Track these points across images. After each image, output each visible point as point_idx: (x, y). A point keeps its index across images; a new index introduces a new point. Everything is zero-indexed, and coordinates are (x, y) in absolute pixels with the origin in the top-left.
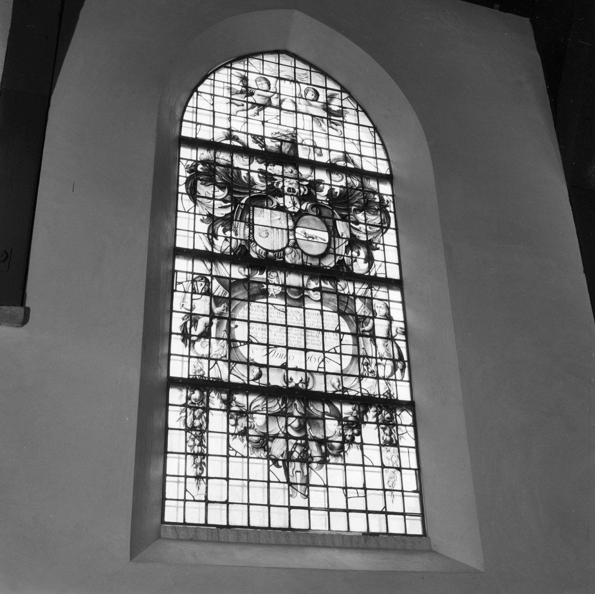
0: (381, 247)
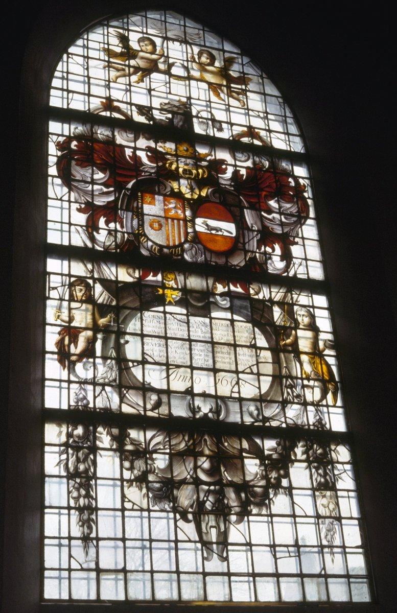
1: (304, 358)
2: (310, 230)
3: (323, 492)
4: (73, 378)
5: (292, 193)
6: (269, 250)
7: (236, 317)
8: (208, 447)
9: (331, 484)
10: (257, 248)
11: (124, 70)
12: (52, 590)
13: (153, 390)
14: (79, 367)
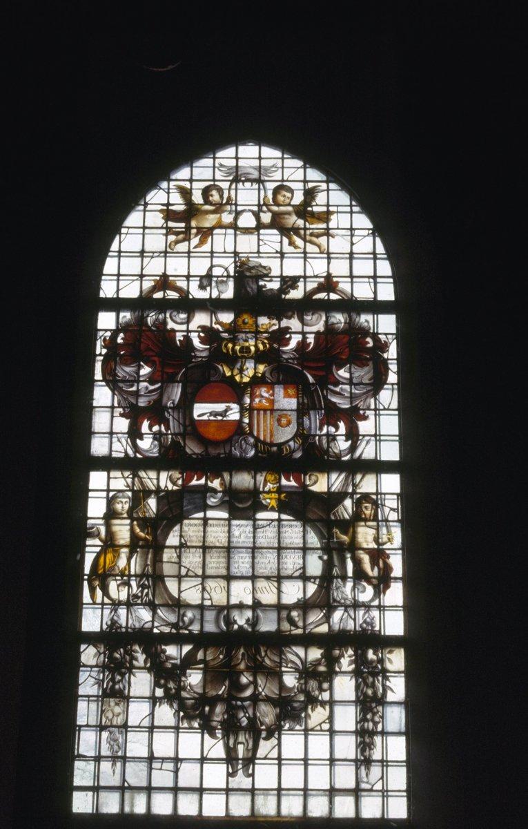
0: (370, 413)
2: (388, 397)
6: (332, 429)
7: (284, 517)
12: (81, 804)
13: (189, 606)
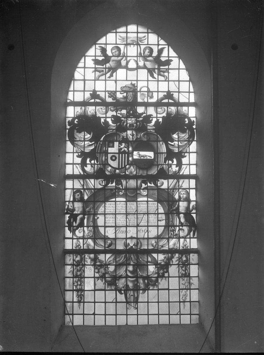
1: (182, 216)
3: (183, 278)
4: (74, 237)
5: (186, 128)
6: (170, 162)
7: (149, 199)
8: (133, 261)
9: (187, 274)
10: (164, 162)
11: (103, 71)
14: (77, 232)
